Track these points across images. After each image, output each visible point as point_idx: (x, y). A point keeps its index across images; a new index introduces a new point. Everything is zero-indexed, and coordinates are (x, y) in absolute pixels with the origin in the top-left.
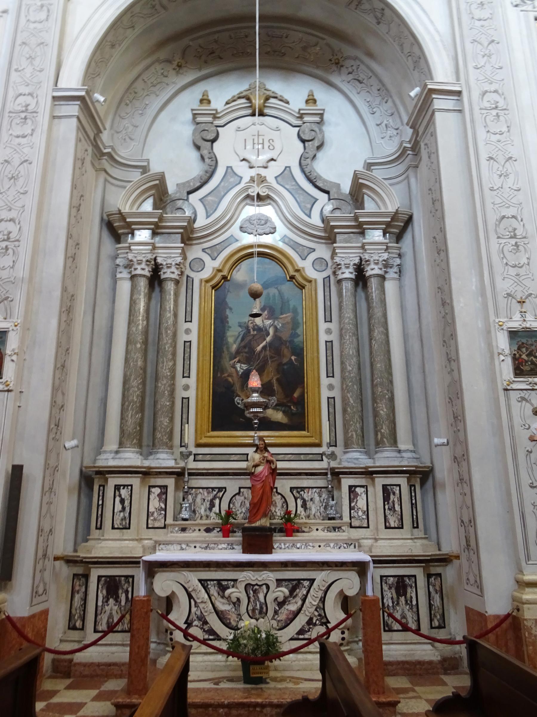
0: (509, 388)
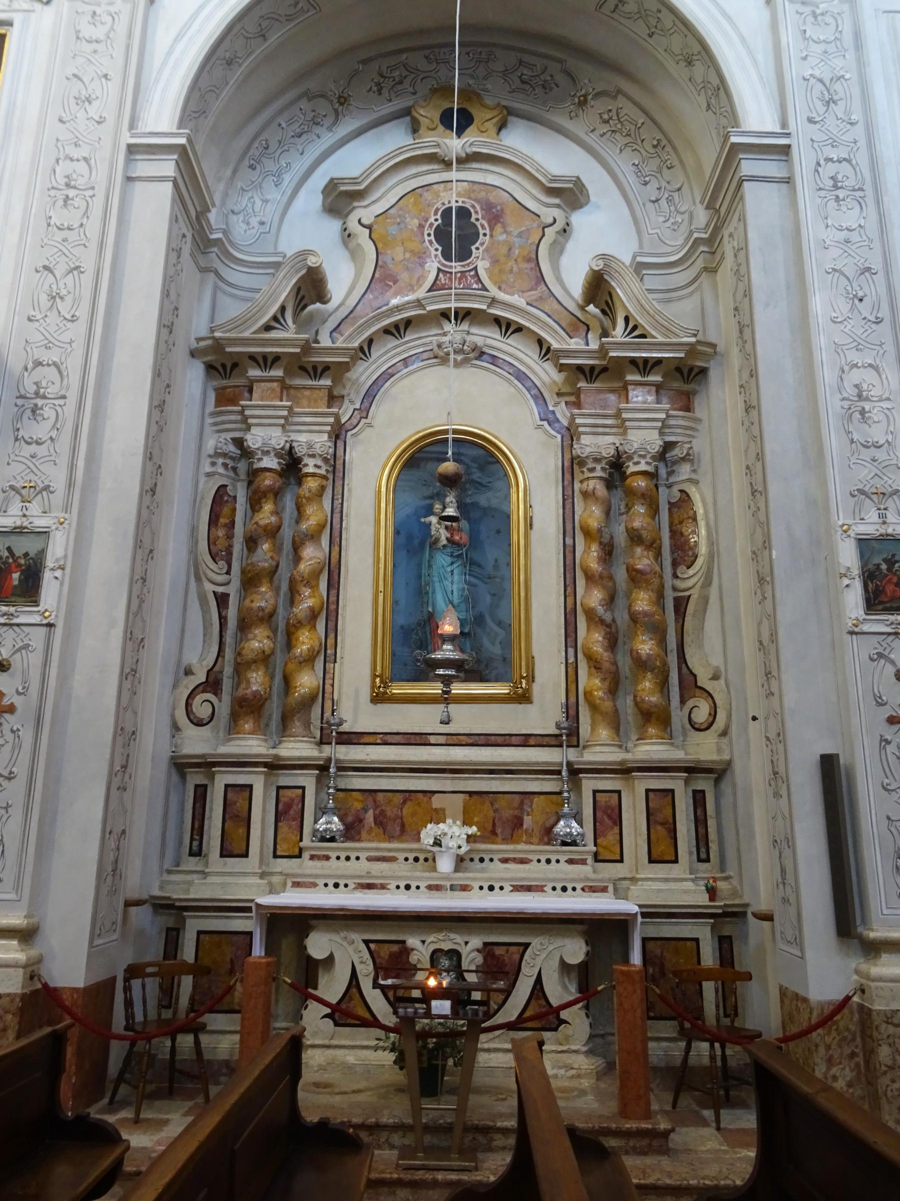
0: (856, 630)
